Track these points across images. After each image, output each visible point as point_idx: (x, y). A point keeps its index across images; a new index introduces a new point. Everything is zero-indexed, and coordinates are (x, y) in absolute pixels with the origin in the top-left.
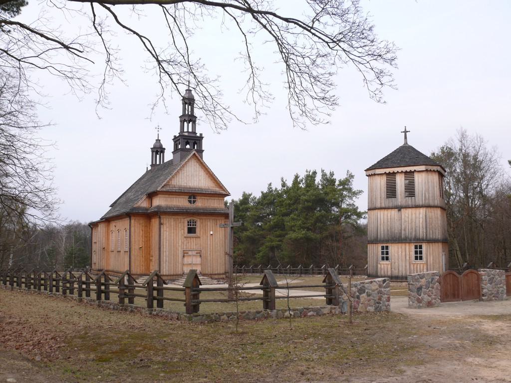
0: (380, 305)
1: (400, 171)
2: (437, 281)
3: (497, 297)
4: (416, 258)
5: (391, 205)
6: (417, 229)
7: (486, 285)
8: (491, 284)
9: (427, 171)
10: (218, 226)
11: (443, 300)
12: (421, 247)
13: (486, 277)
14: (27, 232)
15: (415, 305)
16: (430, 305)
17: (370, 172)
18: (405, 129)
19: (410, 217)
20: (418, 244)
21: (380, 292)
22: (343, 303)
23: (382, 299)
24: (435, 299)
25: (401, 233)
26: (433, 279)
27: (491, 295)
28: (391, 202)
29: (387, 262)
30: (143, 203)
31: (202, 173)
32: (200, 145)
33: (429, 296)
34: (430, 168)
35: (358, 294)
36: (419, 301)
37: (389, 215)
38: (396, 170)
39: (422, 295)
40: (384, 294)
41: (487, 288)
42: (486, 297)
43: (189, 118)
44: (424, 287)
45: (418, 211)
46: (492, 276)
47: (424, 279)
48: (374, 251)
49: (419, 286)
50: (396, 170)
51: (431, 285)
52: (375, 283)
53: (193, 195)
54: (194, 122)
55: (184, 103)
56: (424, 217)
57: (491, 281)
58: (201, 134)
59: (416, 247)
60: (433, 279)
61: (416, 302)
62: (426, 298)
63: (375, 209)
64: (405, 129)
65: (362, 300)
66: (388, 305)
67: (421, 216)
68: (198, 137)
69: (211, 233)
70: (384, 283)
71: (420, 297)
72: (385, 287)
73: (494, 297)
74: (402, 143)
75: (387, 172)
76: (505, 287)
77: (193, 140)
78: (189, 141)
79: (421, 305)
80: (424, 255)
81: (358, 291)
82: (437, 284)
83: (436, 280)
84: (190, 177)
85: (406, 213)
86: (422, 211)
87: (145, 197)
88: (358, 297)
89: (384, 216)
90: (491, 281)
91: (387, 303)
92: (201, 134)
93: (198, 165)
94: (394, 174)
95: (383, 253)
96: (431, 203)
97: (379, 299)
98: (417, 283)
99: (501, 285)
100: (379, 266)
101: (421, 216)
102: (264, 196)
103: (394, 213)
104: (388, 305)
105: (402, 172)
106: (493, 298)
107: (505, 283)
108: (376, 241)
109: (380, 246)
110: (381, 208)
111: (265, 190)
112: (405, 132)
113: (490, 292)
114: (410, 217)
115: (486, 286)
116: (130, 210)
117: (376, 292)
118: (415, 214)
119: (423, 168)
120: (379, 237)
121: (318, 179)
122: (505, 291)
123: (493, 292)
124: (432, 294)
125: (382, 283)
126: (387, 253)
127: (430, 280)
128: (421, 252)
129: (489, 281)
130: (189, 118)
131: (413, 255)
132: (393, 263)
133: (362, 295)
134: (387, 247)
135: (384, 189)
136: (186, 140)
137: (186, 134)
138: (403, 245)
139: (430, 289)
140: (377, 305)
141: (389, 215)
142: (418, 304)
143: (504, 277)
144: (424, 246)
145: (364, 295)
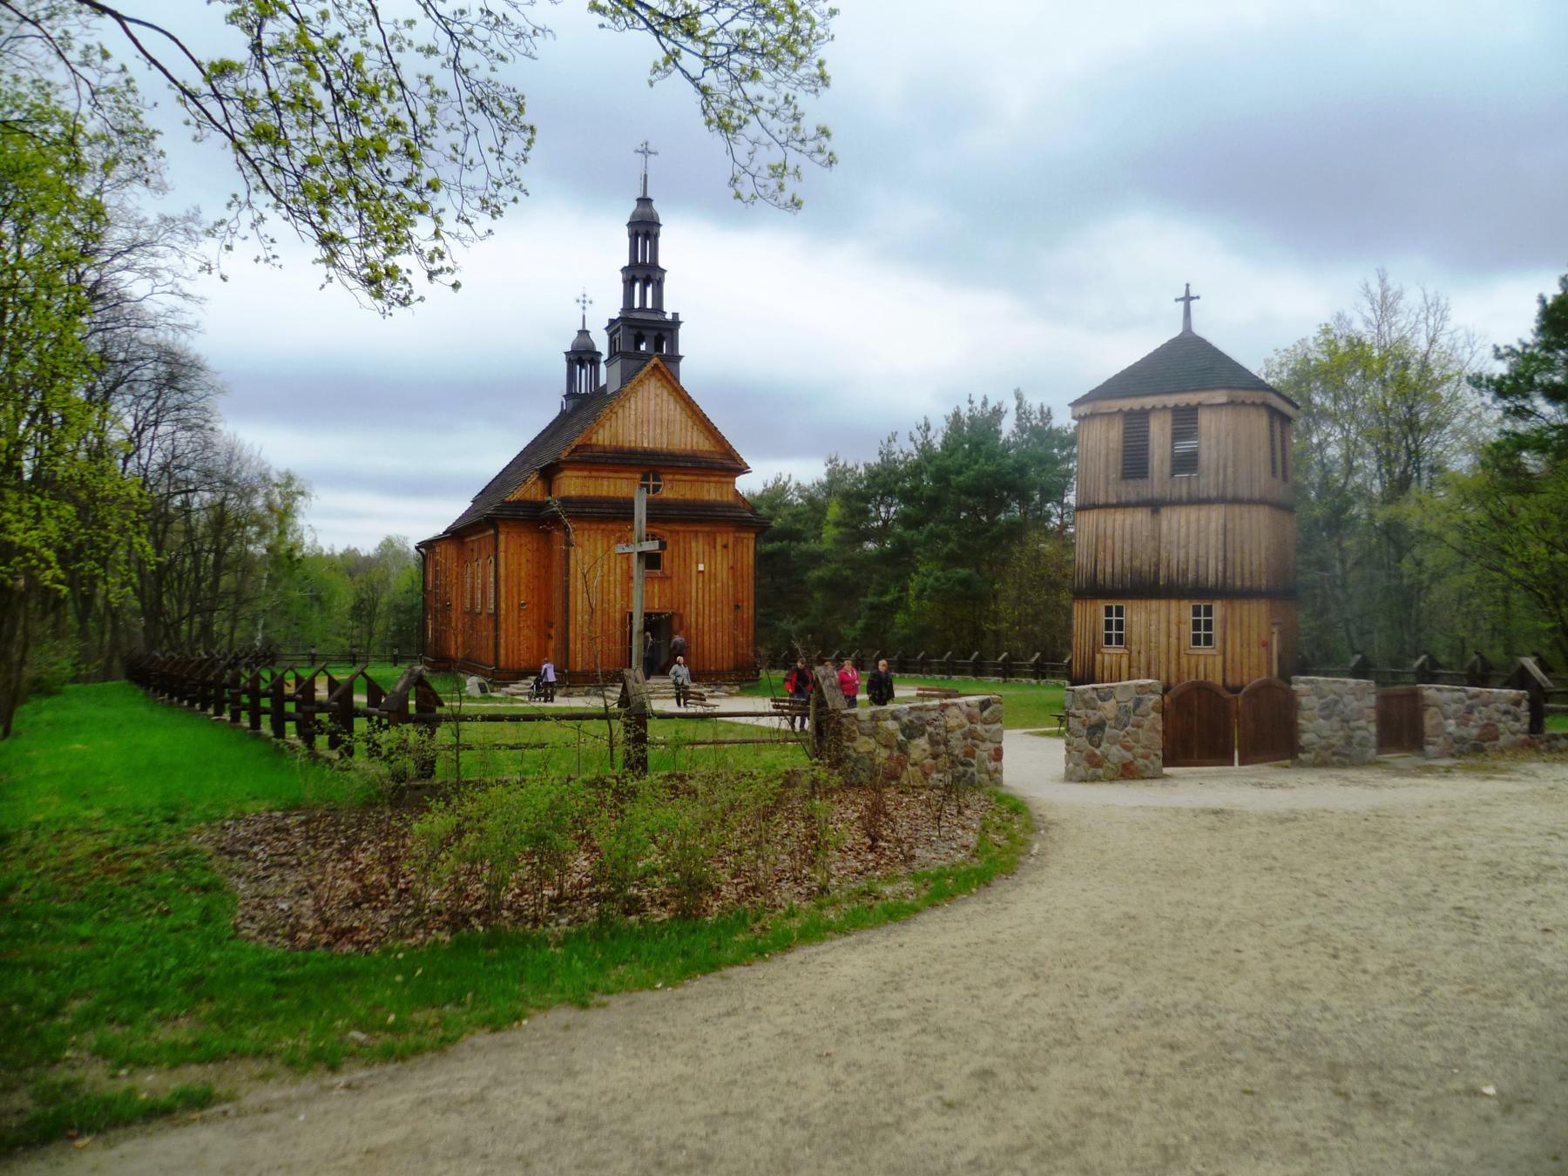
0: (970, 770)
1: (1249, 401)
2: (1154, 709)
3: (1346, 756)
4: (1196, 640)
5: (1133, 498)
6: (1202, 560)
7: (1310, 721)
8: (1327, 718)
9: (1231, 403)
10: (719, 547)
11: (1169, 761)
12: (1209, 611)
13: (1315, 698)
14: (287, 561)
15: (1081, 771)
16: (1127, 773)
17: (1083, 410)
18: (1187, 291)
19: (1183, 530)
20: (1203, 604)
21: (971, 734)
22: (856, 761)
23: (978, 752)
24: (1145, 757)
25: (1157, 573)
26: (1138, 702)
27: (1325, 748)
28: (1131, 491)
29: (1120, 650)
30: (531, 490)
31: (673, 409)
32: (674, 344)
33: (1127, 748)
34: (1241, 395)
35: (901, 737)
36: (1094, 761)
37: (1128, 522)
38: (1149, 402)
39: (1104, 745)
40: (984, 741)
41: (1313, 727)
42: (1311, 756)
43: (643, 272)
44: (1112, 723)
45: (1204, 511)
46: (1332, 696)
47: (1113, 701)
48: (1088, 617)
49: (1094, 720)
50: (1149, 402)
51: (1133, 719)
52: (955, 711)
53: (651, 464)
54: (659, 285)
55: (634, 237)
56: (1220, 531)
57: (1328, 710)
58: (675, 315)
59: (1196, 612)
60: (1138, 702)
61: (1085, 764)
62: (1116, 753)
63: (1095, 506)
64: (1187, 291)
65: (915, 754)
66: (996, 771)
67: (1213, 525)
68: (667, 322)
69: (701, 567)
70: (982, 711)
71: (1098, 752)
72: (985, 722)
73: (1334, 754)
74: (1175, 331)
75: (1126, 408)
76: (1373, 728)
77: (652, 329)
78: (644, 332)
79: (1100, 771)
80: (1216, 632)
81: (903, 731)
82: (1153, 714)
83: (1150, 704)
84: (643, 421)
85: (1176, 521)
86: (1216, 514)
87: (534, 477)
88: (902, 748)
89: (1121, 524)
90: (1328, 710)
91: (991, 765)
92: (675, 315)
93: (665, 394)
94: (1144, 414)
95: (1196, 625)
96: (1244, 493)
97: (967, 754)
98: (1090, 712)
99: (1362, 723)
100: (1098, 657)
101: (1213, 525)
102: (873, 474)
103: (1141, 517)
104: (996, 771)
105: (1165, 407)
106: (1335, 758)
107: (1374, 716)
108: (1093, 590)
109: (1101, 605)
110: (1107, 506)
111: (875, 460)
112: (1188, 299)
113: (1323, 742)
114: (1183, 530)
115: (1310, 725)
116: (497, 509)
117: (958, 733)
118: (1198, 520)
119: (1220, 397)
120: (1100, 576)
121: (1008, 426)
122: (1373, 739)
123: (1334, 741)
124: (1137, 742)
125: (977, 710)
126: (1120, 625)
127: (1131, 704)
128: (1208, 625)
129: (1322, 710)
130: (643, 272)
131: (1188, 631)
132: (1134, 654)
133: (916, 742)
134: (1120, 612)
135: (1116, 458)
136: (635, 332)
137: (637, 316)
138: (1163, 603)
139: (1129, 728)
140: (961, 768)
141: (1128, 522)
142: (1091, 770)
143: (1372, 700)
144: (1218, 608)
145: (922, 742)
